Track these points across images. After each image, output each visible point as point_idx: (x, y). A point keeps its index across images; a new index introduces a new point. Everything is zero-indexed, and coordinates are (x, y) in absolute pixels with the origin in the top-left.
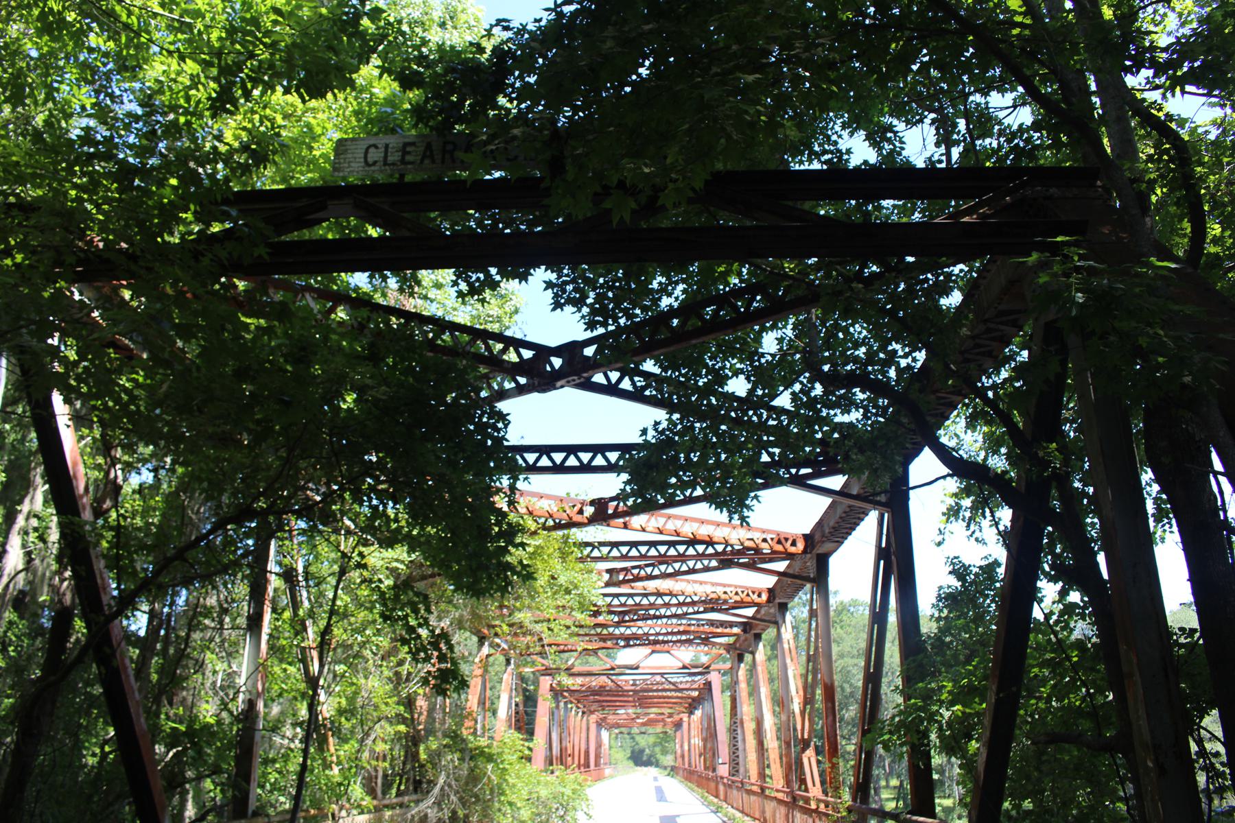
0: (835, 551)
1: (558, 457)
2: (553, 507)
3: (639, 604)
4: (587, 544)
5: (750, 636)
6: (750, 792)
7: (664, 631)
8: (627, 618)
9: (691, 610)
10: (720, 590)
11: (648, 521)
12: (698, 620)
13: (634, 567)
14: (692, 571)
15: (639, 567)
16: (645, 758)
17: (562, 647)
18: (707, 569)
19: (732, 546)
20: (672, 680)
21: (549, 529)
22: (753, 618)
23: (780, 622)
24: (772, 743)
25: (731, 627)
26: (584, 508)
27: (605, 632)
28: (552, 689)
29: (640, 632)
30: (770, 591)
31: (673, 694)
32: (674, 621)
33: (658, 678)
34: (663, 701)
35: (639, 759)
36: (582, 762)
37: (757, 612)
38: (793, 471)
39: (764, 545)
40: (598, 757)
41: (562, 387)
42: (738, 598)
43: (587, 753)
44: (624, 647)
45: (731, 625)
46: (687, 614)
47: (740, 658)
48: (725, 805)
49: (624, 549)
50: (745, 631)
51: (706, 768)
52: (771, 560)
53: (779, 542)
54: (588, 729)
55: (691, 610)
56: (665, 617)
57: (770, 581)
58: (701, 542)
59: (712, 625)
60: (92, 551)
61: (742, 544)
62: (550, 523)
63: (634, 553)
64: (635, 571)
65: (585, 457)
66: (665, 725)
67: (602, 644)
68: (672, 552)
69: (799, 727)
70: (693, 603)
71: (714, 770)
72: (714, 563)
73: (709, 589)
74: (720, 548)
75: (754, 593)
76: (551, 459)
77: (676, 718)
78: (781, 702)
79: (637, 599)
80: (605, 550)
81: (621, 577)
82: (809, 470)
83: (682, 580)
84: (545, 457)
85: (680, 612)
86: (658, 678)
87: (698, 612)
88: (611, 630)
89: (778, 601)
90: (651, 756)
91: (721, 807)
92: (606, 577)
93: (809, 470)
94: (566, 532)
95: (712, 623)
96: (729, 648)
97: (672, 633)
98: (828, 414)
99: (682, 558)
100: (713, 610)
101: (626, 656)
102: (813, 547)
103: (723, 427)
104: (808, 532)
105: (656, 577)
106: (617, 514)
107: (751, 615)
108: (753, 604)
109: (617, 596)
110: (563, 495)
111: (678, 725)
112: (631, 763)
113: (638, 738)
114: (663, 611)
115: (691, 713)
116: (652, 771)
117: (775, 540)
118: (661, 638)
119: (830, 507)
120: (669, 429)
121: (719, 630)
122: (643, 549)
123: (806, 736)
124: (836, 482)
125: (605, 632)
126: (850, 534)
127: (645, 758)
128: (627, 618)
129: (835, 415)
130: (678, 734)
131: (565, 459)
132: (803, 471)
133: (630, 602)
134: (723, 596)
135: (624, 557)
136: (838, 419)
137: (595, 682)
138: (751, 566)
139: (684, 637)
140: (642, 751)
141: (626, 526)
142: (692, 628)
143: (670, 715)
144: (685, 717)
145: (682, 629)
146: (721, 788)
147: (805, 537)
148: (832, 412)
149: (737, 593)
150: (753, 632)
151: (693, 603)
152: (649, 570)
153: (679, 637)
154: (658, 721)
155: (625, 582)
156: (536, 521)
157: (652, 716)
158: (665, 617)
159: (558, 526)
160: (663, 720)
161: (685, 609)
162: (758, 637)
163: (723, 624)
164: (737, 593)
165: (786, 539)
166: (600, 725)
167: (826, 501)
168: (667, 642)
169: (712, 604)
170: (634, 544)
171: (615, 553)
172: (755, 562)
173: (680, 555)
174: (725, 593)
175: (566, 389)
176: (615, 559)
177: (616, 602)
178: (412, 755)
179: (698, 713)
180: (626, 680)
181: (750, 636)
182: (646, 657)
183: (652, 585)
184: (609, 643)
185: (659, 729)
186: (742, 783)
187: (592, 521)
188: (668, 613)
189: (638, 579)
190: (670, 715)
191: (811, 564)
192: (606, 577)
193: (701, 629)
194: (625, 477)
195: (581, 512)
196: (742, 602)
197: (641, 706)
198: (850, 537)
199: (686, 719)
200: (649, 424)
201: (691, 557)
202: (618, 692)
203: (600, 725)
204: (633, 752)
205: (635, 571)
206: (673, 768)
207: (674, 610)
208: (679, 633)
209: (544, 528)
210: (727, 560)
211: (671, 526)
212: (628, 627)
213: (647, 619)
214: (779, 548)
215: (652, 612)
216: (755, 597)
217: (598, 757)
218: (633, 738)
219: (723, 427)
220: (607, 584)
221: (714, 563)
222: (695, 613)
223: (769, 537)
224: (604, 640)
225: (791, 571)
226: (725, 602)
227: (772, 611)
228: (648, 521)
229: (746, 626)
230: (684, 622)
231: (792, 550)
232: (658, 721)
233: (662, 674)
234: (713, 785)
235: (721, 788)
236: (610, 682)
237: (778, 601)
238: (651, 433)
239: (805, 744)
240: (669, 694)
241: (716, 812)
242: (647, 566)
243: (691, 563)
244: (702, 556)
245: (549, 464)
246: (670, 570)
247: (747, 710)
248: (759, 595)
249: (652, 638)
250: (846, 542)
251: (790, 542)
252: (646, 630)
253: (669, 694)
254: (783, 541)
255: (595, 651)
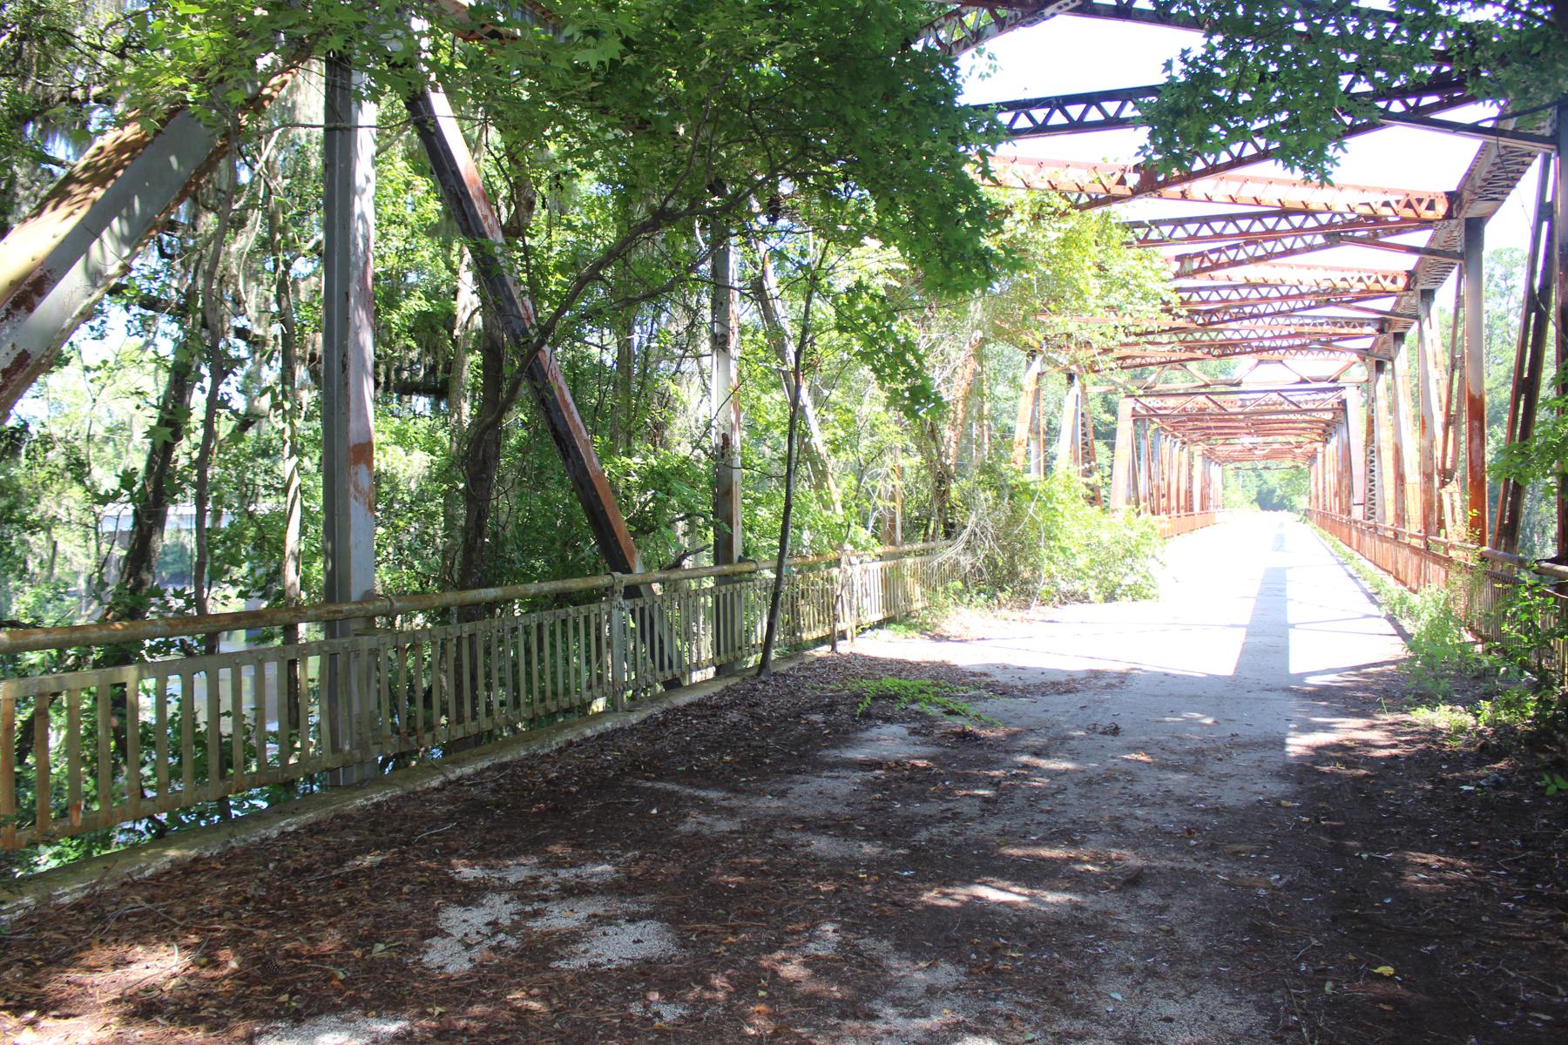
0: (1493, 213)
1: (1075, 111)
2: (1084, 178)
3: (1227, 300)
4: (1139, 225)
5: (1388, 336)
6: (1383, 539)
7: (1269, 334)
8: (1214, 319)
9: (1300, 305)
10: (1336, 278)
11: (1216, 187)
12: (1315, 317)
13: (1212, 251)
14: (1291, 252)
15: (1219, 250)
16: (1275, 500)
17: (1138, 361)
18: (1310, 248)
19: (1341, 214)
20: (1294, 399)
21: (1082, 208)
22: (1392, 313)
23: (1423, 316)
24: (1413, 478)
25: (1361, 325)
26: (1127, 176)
27: (1190, 338)
28: (1135, 414)
29: (1237, 336)
30: (1410, 275)
31: (1298, 417)
32: (1281, 320)
33: (1274, 396)
34: (1285, 427)
35: (1266, 501)
36: (1182, 503)
37: (1397, 303)
38: (1411, 102)
39: (1386, 211)
40: (1205, 498)
41: (1053, 15)
42: (1362, 286)
43: (1189, 493)
44: (1219, 356)
45: (1362, 323)
46: (1294, 310)
47: (1380, 367)
48: (1357, 556)
49: (1192, 228)
50: (1381, 331)
51: (1341, 511)
52: (1399, 232)
53: (1409, 205)
54: (1191, 466)
55: (1300, 305)
56: (1265, 315)
57: (1410, 261)
58: (1296, 212)
59: (1335, 324)
60: (508, 278)
61: (1352, 211)
62: (1084, 200)
63: (1205, 231)
64: (1214, 257)
65: (1094, 115)
66: (1295, 457)
67: (1189, 355)
68: (1258, 227)
69: (1438, 453)
70: (1301, 296)
71: (1349, 513)
72: (1320, 240)
73: (1319, 275)
74: (1324, 219)
75: (1385, 277)
76: (1065, 114)
77: (1309, 447)
78: (1424, 424)
79: (1224, 293)
80: (1166, 230)
81: (1196, 265)
82: (1434, 99)
83: (1281, 265)
84: (1057, 113)
85: (1285, 308)
86: (1274, 396)
87: (1310, 308)
88: (1197, 335)
89: (1419, 287)
90: (1283, 497)
91: (1352, 558)
92: (1176, 266)
93: (1434, 99)
94: (1105, 209)
95: (1334, 322)
96: (1364, 354)
97: (1280, 337)
98: (1449, 11)
99: (1271, 235)
100: (1328, 303)
101: (1241, 366)
102: (1460, 207)
103: (1287, 48)
104: (1453, 188)
105: (1241, 263)
106: (1168, 183)
107: (1388, 309)
108: (1389, 294)
109: (1198, 290)
110: (1097, 160)
111: (1312, 457)
112: (1256, 506)
113: (1266, 474)
114: (1262, 308)
115: (1326, 441)
116: (1282, 515)
117: (1403, 203)
118: (1267, 343)
119: (1481, 150)
120: (1203, 58)
121: (1345, 331)
122: (1218, 226)
123: (1448, 465)
124: (1482, 112)
125: (1190, 338)
126: (1513, 187)
127: (1275, 500)
128: (1214, 319)
129: (1461, 12)
130: (1313, 469)
131: (1085, 112)
132: (1427, 100)
133: (1215, 297)
134: (1341, 285)
135: (1193, 238)
136: (1463, 19)
137: (1193, 404)
138: (1372, 242)
139: (1297, 342)
140: (1272, 492)
141: (1184, 196)
142: (1306, 329)
143: (1299, 445)
144: (1319, 446)
145: (1292, 330)
146: (1354, 533)
147: (1451, 196)
148: (1456, 9)
149: (1360, 280)
150: (1392, 331)
151: (1301, 296)
152: (1232, 253)
153: (1291, 342)
154: (1284, 452)
155: (1201, 270)
156: (1065, 197)
157: (1275, 446)
158: (1265, 315)
159: (1095, 203)
160: (1290, 451)
161: (1292, 303)
162: (1399, 337)
163: (1348, 322)
164: (1360, 280)
165: (1420, 201)
166: (1209, 457)
167: (1472, 145)
168: (1275, 349)
169: (1329, 296)
170: (1206, 220)
171: (1180, 233)
172: (1376, 235)
173: (1268, 231)
174: (1344, 279)
175: (1058, 17)
176: (1205, 239)
177: (1195, 298)
178: (941, 494)
179: (1334, 441)
180: (1232, 404)
181: (1388, 336)
182: (1251, 369)
183: (1238, 274)
184: (1199, 354)
185: (1288, 463)
186: (1376, 528)
187: (1136, 192)
188: (1270, 310)
189: (1217, 266)
190: (1299, 445)
191: (1457, 231)
192: (1176, 266)
193: (1319, 329)
194: (1145, 130)
195: (1122, 181)
196: (1368, 291)
197: (1258, 433)
198: (1513, 192)
199: (1320, 449)
200: (1175, 55)
201: (1286, 234)
202: (1223, 416)
203: (1209, 457)
204: (1259, 493)
205: (1214, 257)
206: (1307, 513)
207: (1277, 305)
208: (1290, 336)
209: (1076, 206)
210: (1336, 234)
211: (1248, 192)
212: (1220, 331)
213: (1242, 319)
214: (1409, 213)
215: (1248, 310)
216: (1388, 286)
217: (1205, 498)
218: (1259, 476)
219: (1287, 48)
220: (1178, 276)
221: (1320, 240)
222: (1305, 309)
223: (1392, 199)
224: (1192, 349)
225: (1434, 246)
226: (1346, 291)
227: (1413, 301)
228: (1216, 187)
229: (1383, 325)
230: (1294, 321)
231: (1429, 215)
232: (1284, 452)
233: (1279, 392)
234: (1346, 530)
235: (1354, 533)
236: (1211, 405)
237: (1420, 289)
238: (1178, 66)
239: (1446, 475)
240: (1292, 417)
241: (1342, 564)
242: (1229, 248)
243: (1288, 242)
244: (1298, 231)
245: (1064, 121)
246: (1260, 252)
247: (1384, 436)
248: (1394, 281)
249: (1254, 344)
250: (1508, 199)
251: (1424, 204)
252: (1244, 334)
253: (1292, 417)
254: (1415, 203)
255: (1182, 362)
